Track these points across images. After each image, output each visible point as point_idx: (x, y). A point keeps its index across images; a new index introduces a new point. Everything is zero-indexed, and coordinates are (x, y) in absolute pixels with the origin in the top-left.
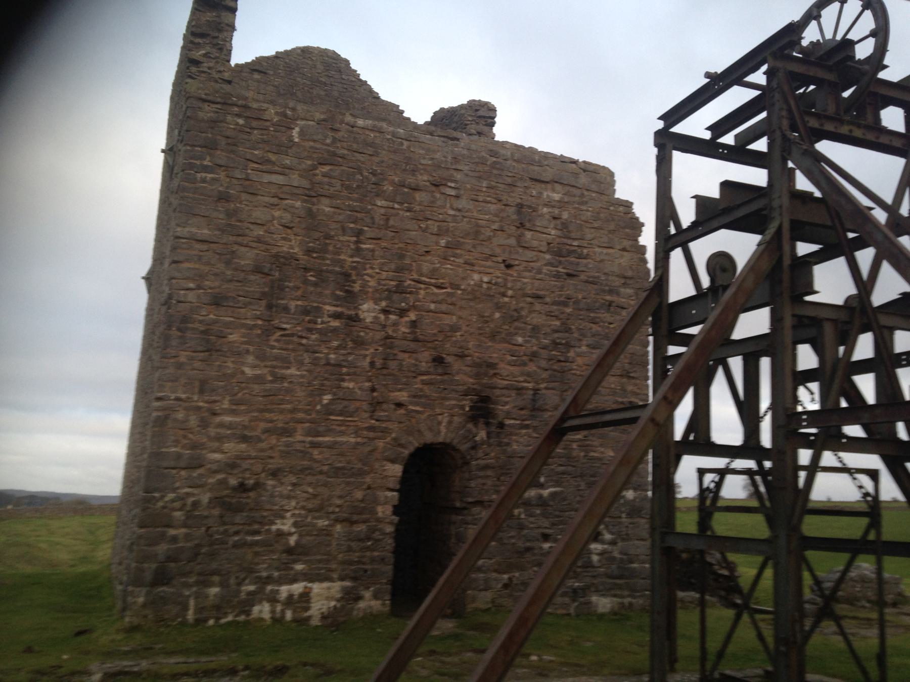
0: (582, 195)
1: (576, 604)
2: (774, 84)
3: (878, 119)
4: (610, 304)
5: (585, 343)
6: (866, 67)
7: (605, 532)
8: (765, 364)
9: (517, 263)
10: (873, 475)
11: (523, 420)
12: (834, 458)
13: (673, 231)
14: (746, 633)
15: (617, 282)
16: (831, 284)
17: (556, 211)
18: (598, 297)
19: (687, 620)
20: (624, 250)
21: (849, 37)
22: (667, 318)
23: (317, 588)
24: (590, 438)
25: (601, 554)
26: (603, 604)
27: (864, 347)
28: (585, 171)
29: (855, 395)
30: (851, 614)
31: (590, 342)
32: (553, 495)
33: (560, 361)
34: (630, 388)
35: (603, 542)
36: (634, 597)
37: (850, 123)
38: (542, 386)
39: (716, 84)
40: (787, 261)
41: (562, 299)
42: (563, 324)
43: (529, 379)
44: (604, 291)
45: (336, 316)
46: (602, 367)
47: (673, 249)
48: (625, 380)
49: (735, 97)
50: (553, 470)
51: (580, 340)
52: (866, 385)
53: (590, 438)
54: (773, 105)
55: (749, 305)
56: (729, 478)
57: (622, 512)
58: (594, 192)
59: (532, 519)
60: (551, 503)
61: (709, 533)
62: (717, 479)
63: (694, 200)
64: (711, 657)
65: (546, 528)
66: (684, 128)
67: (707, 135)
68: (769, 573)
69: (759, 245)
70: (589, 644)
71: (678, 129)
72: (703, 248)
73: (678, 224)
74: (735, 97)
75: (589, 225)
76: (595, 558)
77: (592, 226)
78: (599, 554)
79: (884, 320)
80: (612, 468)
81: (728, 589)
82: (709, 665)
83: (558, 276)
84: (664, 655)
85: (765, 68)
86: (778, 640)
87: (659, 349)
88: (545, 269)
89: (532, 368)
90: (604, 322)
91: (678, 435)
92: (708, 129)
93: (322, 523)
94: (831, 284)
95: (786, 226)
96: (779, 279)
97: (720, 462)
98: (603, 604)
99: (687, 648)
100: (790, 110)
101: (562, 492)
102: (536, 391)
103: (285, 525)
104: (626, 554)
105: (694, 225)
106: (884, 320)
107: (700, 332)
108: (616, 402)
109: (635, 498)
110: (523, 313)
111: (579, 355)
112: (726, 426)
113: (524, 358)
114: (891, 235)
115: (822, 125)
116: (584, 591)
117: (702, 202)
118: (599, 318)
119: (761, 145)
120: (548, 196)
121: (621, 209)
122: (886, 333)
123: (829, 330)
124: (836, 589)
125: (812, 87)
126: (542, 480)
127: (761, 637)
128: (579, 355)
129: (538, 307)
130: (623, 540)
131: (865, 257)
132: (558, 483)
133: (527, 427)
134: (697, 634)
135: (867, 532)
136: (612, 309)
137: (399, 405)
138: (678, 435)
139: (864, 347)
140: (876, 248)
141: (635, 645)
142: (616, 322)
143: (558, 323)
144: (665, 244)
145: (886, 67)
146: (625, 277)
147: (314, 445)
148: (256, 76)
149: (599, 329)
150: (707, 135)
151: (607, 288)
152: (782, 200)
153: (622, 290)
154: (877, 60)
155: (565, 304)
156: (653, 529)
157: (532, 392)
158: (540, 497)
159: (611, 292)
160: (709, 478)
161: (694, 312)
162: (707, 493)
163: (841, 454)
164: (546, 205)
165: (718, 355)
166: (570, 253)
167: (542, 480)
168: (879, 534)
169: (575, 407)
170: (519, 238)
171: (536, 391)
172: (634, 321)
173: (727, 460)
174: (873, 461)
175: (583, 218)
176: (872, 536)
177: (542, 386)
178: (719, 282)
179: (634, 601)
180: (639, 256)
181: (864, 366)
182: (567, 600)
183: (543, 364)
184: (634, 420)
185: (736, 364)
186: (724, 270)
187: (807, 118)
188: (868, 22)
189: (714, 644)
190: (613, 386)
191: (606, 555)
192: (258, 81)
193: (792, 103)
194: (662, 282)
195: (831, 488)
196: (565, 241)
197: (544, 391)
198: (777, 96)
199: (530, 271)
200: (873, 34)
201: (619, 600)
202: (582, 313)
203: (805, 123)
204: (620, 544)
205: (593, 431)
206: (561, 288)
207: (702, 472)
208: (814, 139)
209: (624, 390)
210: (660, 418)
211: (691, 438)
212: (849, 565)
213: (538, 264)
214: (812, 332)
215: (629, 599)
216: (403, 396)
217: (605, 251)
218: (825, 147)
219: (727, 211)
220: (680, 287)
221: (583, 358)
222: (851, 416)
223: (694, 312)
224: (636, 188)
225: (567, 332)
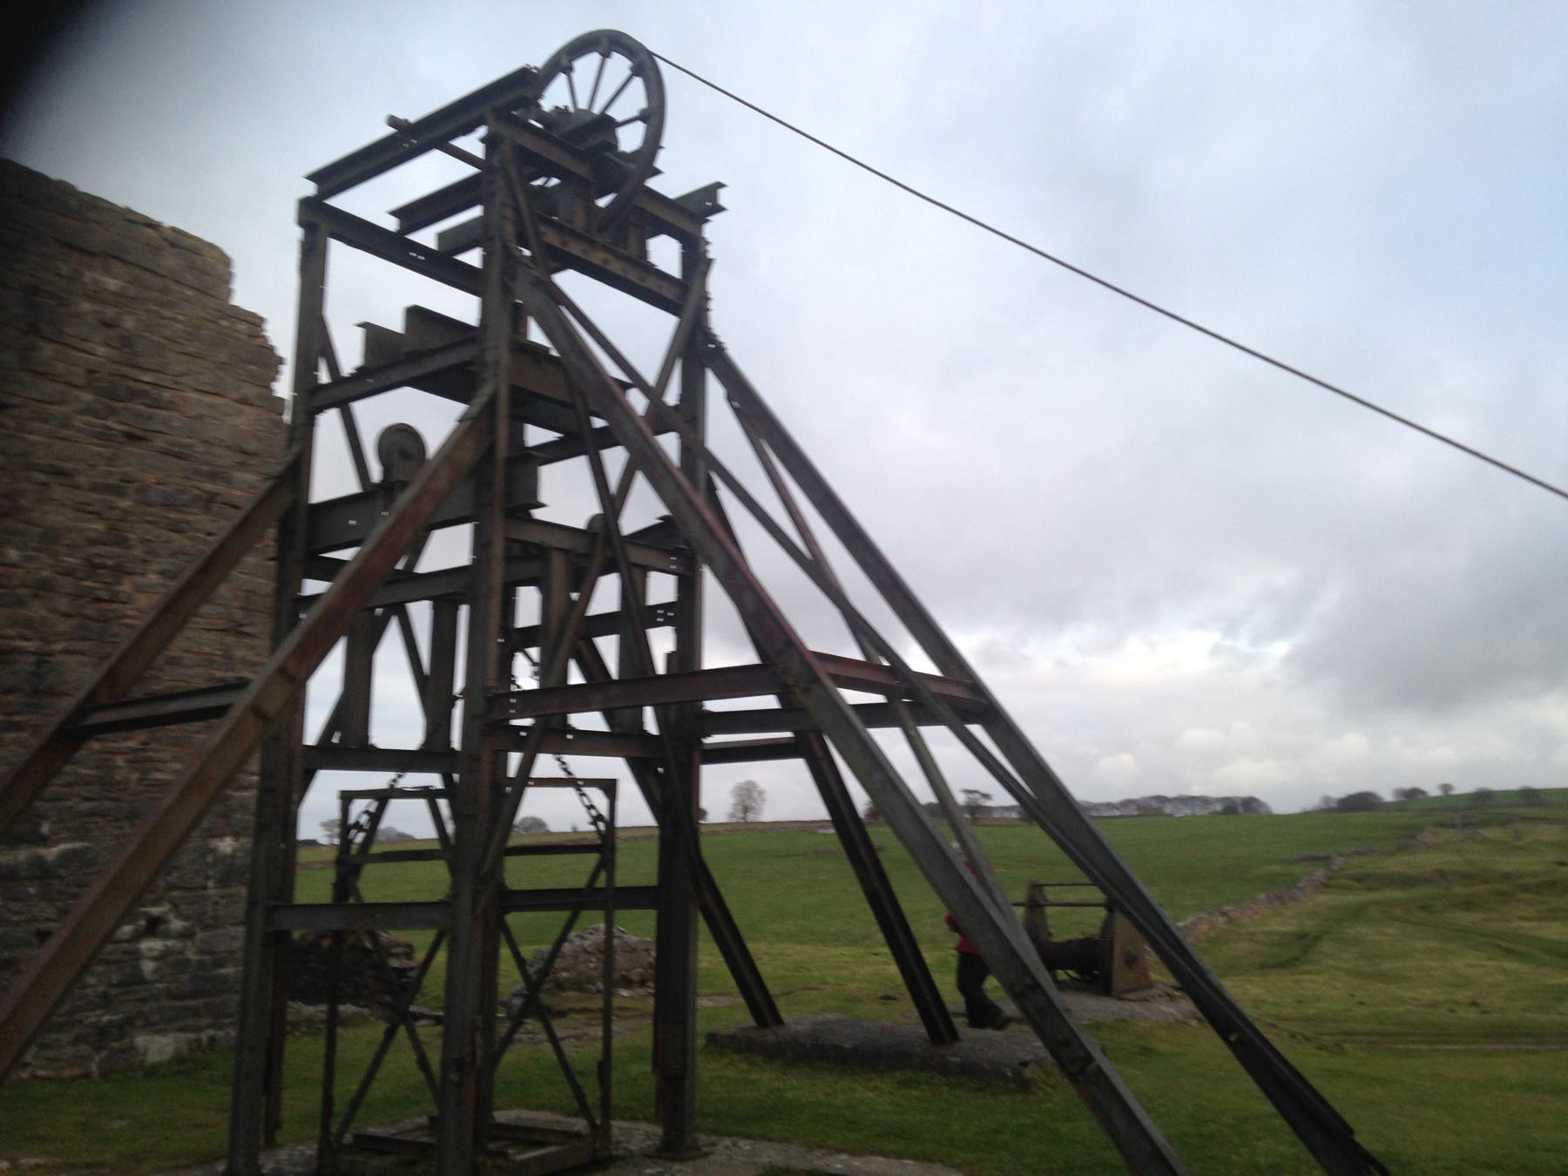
0: (165, 291)
1: (104, 1054)
2: (496, 161)
3: (644, 252)
4: (212, 497)
5: (155, 567)
6: (631, 166)
7: (171, 917)
8: (464, 612)
9: (17, 401)
10: (609, 787)
11: (11, 714)
12: (571, 769)
13: (324, 377)
14: (401, 1058)
15: (230, 459)
16: (566, 495)
17: (110, 312)
18: (188, 483)
19: (302, 1053)
20: (244, 401)
21: (611, 113)
22: (305, 530)
24: (154, 745)
25: (162, 957)
26: (158, 1046)
27: (606, 595)
28: (173, 245)
29: (592, 664)
30: (579, 1006)
31: (165, 567)
32: (66, 857)
33: (99, 600)
34: (240, 653)
35: (166, 936)
36: (221, 1027)
37: (605, 249)
38: (59, 646)
39: (406, 142)
40: (502, 452)
41: (111, 481)
42: (112, 529)
43: (28, 633)
44: (198, 472)
46: (175, 611)
47: (321, 409)
48: (230, 639)
49: (432, 172)
50: (71, 808)
51: (145, 561)
52: (608, 647)
53: (154, 745)
54: (493, 194)
55: (438, 519)
56: (395, 805)
57: (208, 878)
58: (191, 287)
59: (17, 906)
60: (62, 872)
61: (352, 901)
62: (372, 809)
63: (360, 332)
64: (340, 1106)
65: (48, 920)
66: (352, 202)
67: (392, 224)
68: (441, 957)
69: (461, 420)
70: (118, 1124)
71: (340, 202)
72: (377, 413)
73: (334, 367)
74: (432, 172)
75: (178, 349)
76: (148, 967)
77: (178, 349)
78: (154, 959)
79: (636, 555)
80: (168, 800)
81: (396, 994)
82: (335, 1126)
83: (106, 436)
84: (257, 1119)
85: (482, 131)
86: (445, 1064)
87: (286, 583)
88: (79, 421)
89: (37, 610)
90: (197, 530)
91: (311, 736)
92: (394, 213)
94: (566, 495)
95: (504, 394)
96: (489, 480)
97: (379, 780)
98: (158, 1046)
99: (299, 1101)
100: (517, 210)
101: (87, 849)
102: (42, 657)
104: (211, 952)
105: (361, 372)
106: (636, 555)
107: (356, 558)
108: (213, 678)
109: (235, 851)
110: (24, 503)
111: (140, 589)
112: (397, 716)
113: (23, 591)
114: (647, 430)
115: (565, 243)
116: (124, 1027)
117: (375, 336)
118: (187, 522)
119: (473, 258)
120: (95, 282)
121: (242, 327)
122: (637, 573)
123: (558, 565)
124: (545, 972)
125: (554, 181)
126: (45, 828)
127: (423, 1064)
128: (140, 589)
129: (57, 492)
130: (206, 927)
131: (615, 459)
132: (81, 834)
133: (18, 727)
134: (319, 1072)
135: (595, 876)
136: (215, 507)
138: (311, 736)
139: (606, 595)
140: (629, 448)
141: (207, 1112)
142: (214, 527)
143: (100, 526)
144: (312, 398)
145: (657, 172)
146: (243, 452)
149: (185, 542)
150: (392, 224)
151: (205, 468)
152: (498, 352)
153: (237, 475)
154: (646, 159)
155: (118, 492)
156: (252, 903)
157: (32, 659)
158: (40, 861)
159: (213, 476)
160: (359, 807)
161: (352, 522)
162: (353, 832)
163: (566, 758)
164: (88, 297)
165: (392, 596)
166: (133, 395)
167: (45, 828)
168: (611, 878)
169: (112, 690)
171: (42, 657)
172: (244, 531)
173: (391, 775)
174: (615, 767)
175: (167, 333)
176: (601, 882)
177: (59, 646)
178: (397, 475)
179: (220, 1033)
180: (274, 416)
181: (606, 624)
182: (84, 1049)
183: (64, 604)
184: (220, 712)
185: (421, 613)
186: (406, 456)
187: (543, 228)
188: (635, 98)
189: (346, 1087)
190: (207, 650)
191: (171, 959)
193: (521, 198)
194: (299, 469)
195: (552, 809)
197: (60, 658)
198: (500, 183)
199: (45, 421)
200: (643, 117)
201: (192, 1036)
202: (150, 509)
203: (538, 234)
204: (200, 935)
205: (160, 732)
206: (112, 460)
207: (347, 797)
208: (553, 264)
209: (228, 656)
210: (272, 705)
211: (335, 740)
213: (65, 409)
214: (533, 568)
215: (211, 1032)
217: (207, 399)
218: (570, 282)
219: (414, 357)
220: (332, 476)
221: (144, 593)
222: (579, 699)
223: (352, 522)
224: (265, 288)
225: (116, 544)
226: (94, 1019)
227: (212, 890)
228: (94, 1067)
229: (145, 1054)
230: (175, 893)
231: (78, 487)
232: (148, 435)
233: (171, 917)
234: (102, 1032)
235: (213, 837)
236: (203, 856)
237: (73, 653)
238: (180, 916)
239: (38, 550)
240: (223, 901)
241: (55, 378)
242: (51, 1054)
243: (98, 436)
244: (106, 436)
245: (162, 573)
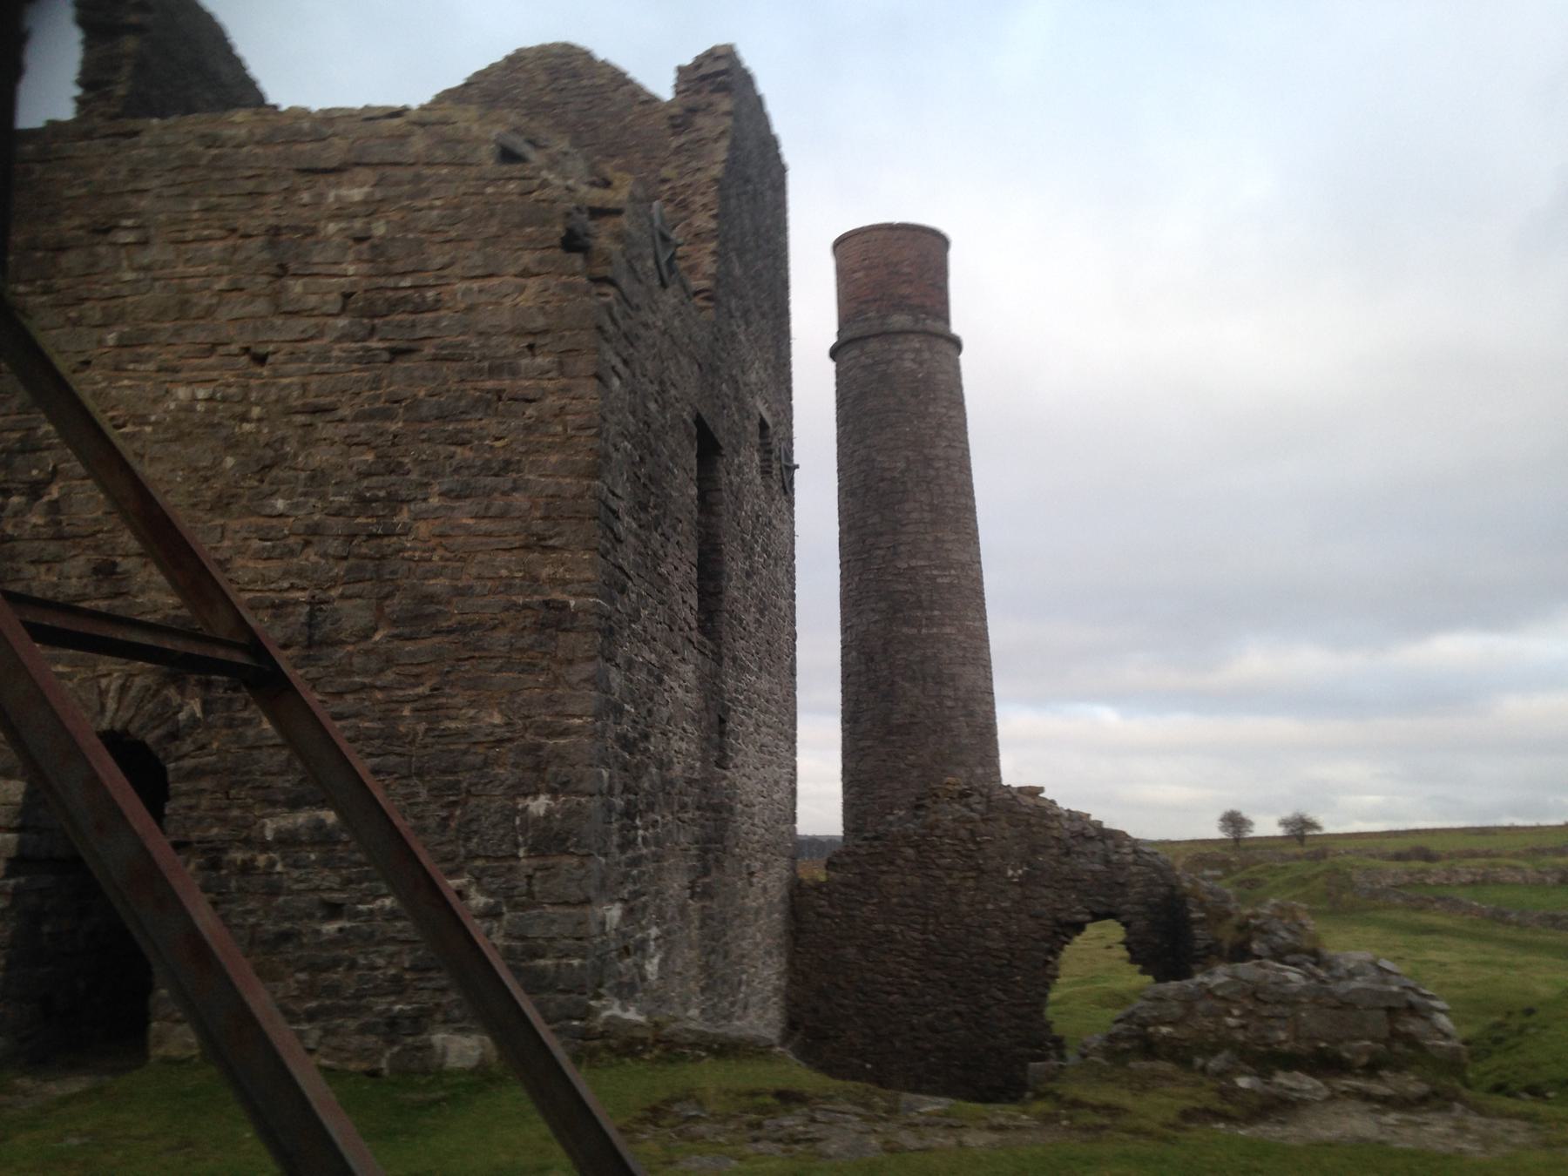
0: (418, 178)
1: (396, 1049)
5: (436, 488)
7: (472, 891)
9: (271, 348)
15: (513, 346)
20: (526, 273)
24: (447, 690)
31: (445, 487)
33: (371, 536)
38: (333, 593)
65: (331, 889)
83: (368, 359)
104: (523, 938)
109: (549, 812)
116: (419, 1021)
118: (470, 431)
120: (338, 198)
130: (515, 907)
143: (370, 457)
155: (388, 415)
159: (494, 371)
166: (393, 306)
170: (275, 297)
175: (422, 226)
182: (371, 1040)
196: (382, 281)
226: (382, 1007)
227: (525, 862)
228: (384, 1064)
229: (444, 1054)
230: (479, 863)
231: (342, 420)
232: (413, 345)
233: (472, 891)
234: (393, 1022)
235: (526, 795)
236: (509, 818)
237: (350, 597)
238: (484, 891)
239: (305, 494)
240: (539, 874)
241: (310, 313)
242: (335, 1041)
243: (359, 360)
244: (368, 359)
245: (441, 494)
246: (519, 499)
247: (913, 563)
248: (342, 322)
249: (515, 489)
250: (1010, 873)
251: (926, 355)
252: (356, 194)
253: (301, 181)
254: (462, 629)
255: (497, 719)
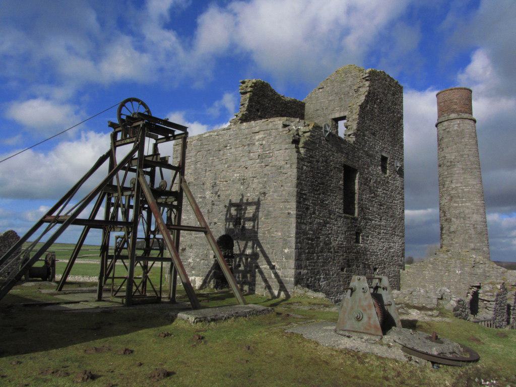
23: (197, 278)
34: (288, 207)
45: (201, 198)
83: (261, 167)
93: (198, 260)
103: (190, 260)
137: (215, 223)
147: (196, 237)
148: (321, 90)
170: (249, 156)
176: (160, 256)
192: (321, 92)
196: (264, 152)
212: (154, 263)
216: (216, 220)
246: (284, 193)
247: (457, 185)
248: (258, 161)
249: (283, 191)
250: (457, 272)
251: (461, 125)
252: (261, 136)
253: (253, 135)
254: (275, 217)
255: (280, 234)
